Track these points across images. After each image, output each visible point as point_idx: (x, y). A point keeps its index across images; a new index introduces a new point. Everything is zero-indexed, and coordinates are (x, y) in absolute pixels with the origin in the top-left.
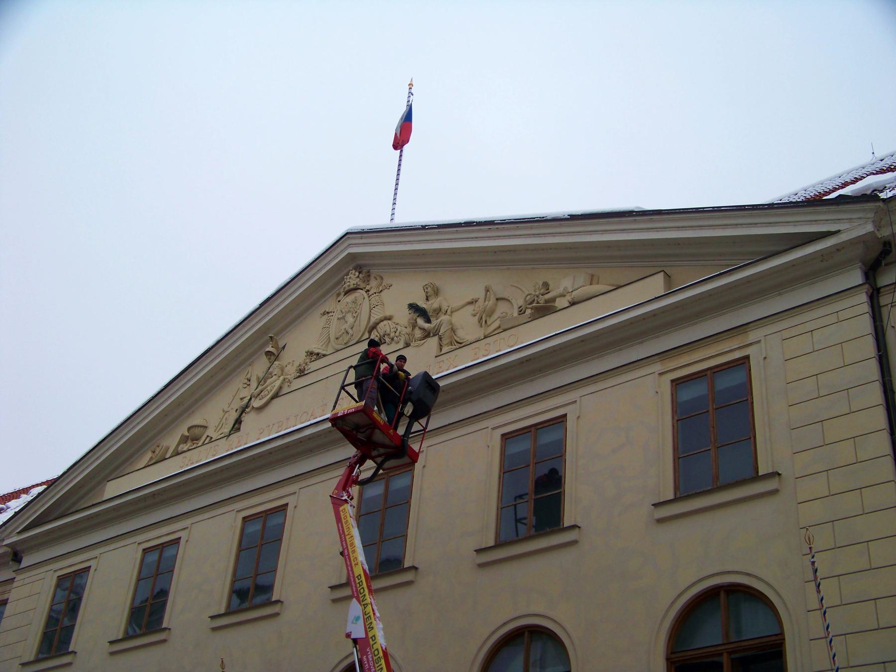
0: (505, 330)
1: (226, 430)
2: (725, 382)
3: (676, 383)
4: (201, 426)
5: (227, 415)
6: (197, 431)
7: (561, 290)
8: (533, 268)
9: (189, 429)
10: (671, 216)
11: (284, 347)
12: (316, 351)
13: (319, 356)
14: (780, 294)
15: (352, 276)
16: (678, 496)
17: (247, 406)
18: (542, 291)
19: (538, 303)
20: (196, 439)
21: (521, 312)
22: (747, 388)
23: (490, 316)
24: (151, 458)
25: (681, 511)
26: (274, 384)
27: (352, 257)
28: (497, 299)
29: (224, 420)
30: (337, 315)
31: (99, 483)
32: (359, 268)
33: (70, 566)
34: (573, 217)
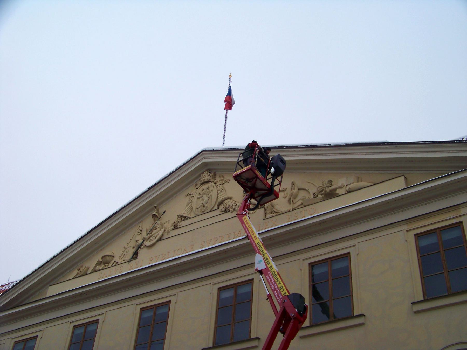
0: (305, 206)
1: (128, 258)
2: (338, 266)
3: (220, 289)
4: (110, 256)
5: (127, 250)
6: (108, 258)
7: (340, 184)
8: (320, 173)
9: (103, 257)
10: (408, 146)
11: (164, 213)
12: (185, 215)
13: (186, 218)
14: (326, 234)
15: (206, 175)
16: (426, 298)
17: (141, 245)
18: (328, 185)
19: (325, 191)
20: (106, 263)
21: (315, 196)
22: (167, 314)
23: (295, 198)
24: (78, 274)
25: (310, 333)
26: (158, 233)
27: (205, 164)
28: (299, 189)
29: (125, 252)
30: (197, 195)
31: (44, 286)
32: (209, 170)
33: (321, 255)
34: (347, 145)
